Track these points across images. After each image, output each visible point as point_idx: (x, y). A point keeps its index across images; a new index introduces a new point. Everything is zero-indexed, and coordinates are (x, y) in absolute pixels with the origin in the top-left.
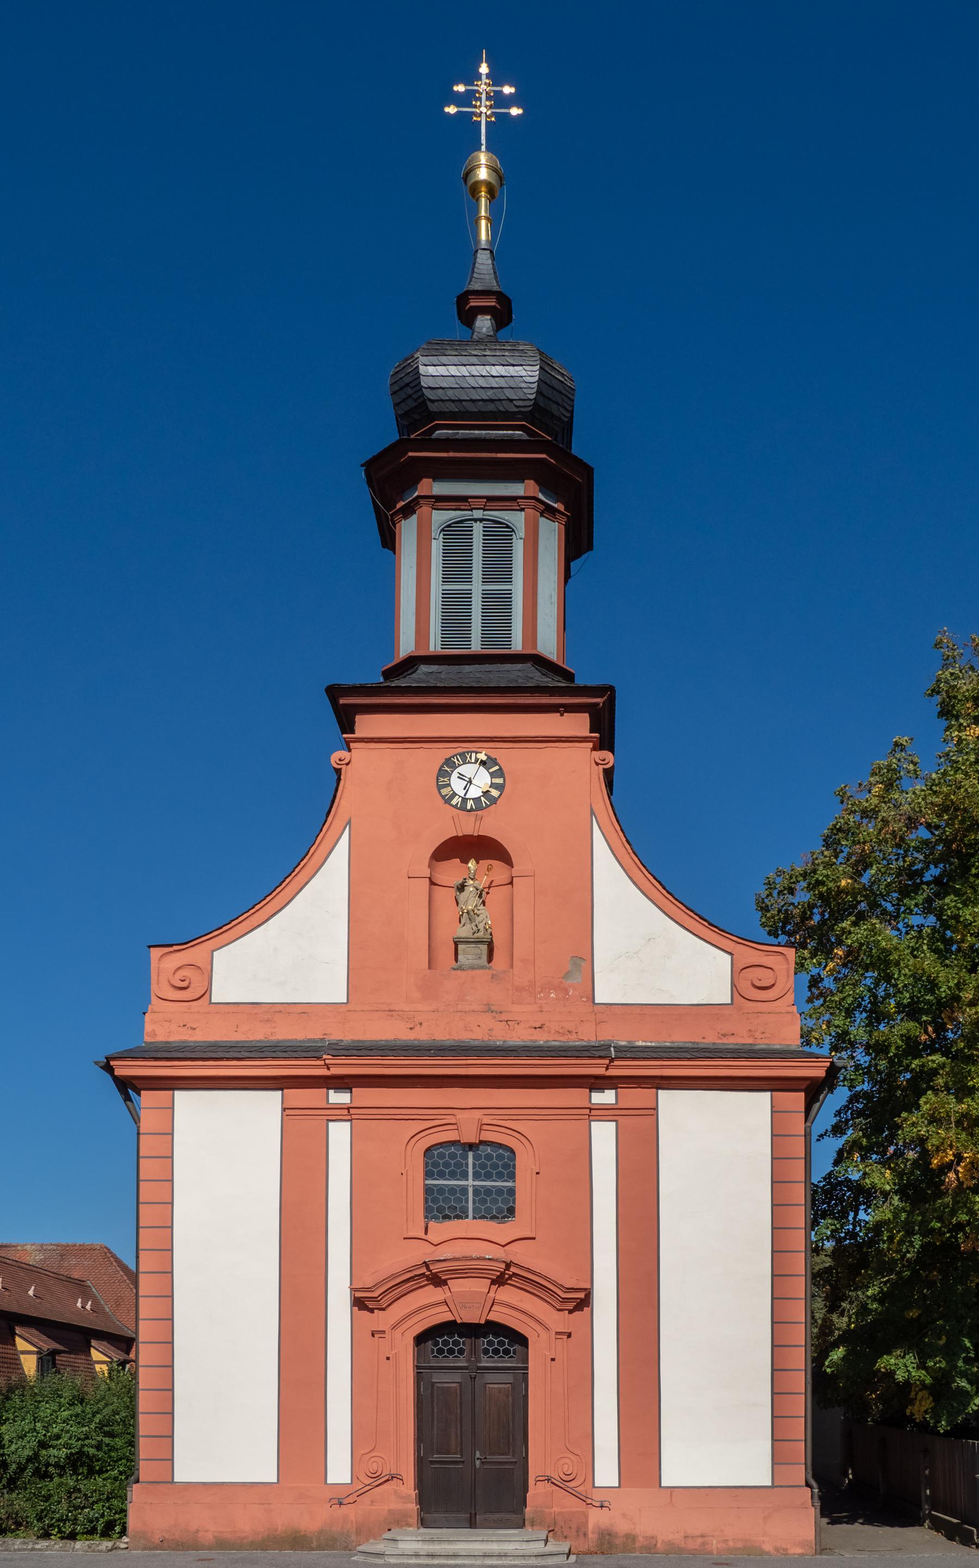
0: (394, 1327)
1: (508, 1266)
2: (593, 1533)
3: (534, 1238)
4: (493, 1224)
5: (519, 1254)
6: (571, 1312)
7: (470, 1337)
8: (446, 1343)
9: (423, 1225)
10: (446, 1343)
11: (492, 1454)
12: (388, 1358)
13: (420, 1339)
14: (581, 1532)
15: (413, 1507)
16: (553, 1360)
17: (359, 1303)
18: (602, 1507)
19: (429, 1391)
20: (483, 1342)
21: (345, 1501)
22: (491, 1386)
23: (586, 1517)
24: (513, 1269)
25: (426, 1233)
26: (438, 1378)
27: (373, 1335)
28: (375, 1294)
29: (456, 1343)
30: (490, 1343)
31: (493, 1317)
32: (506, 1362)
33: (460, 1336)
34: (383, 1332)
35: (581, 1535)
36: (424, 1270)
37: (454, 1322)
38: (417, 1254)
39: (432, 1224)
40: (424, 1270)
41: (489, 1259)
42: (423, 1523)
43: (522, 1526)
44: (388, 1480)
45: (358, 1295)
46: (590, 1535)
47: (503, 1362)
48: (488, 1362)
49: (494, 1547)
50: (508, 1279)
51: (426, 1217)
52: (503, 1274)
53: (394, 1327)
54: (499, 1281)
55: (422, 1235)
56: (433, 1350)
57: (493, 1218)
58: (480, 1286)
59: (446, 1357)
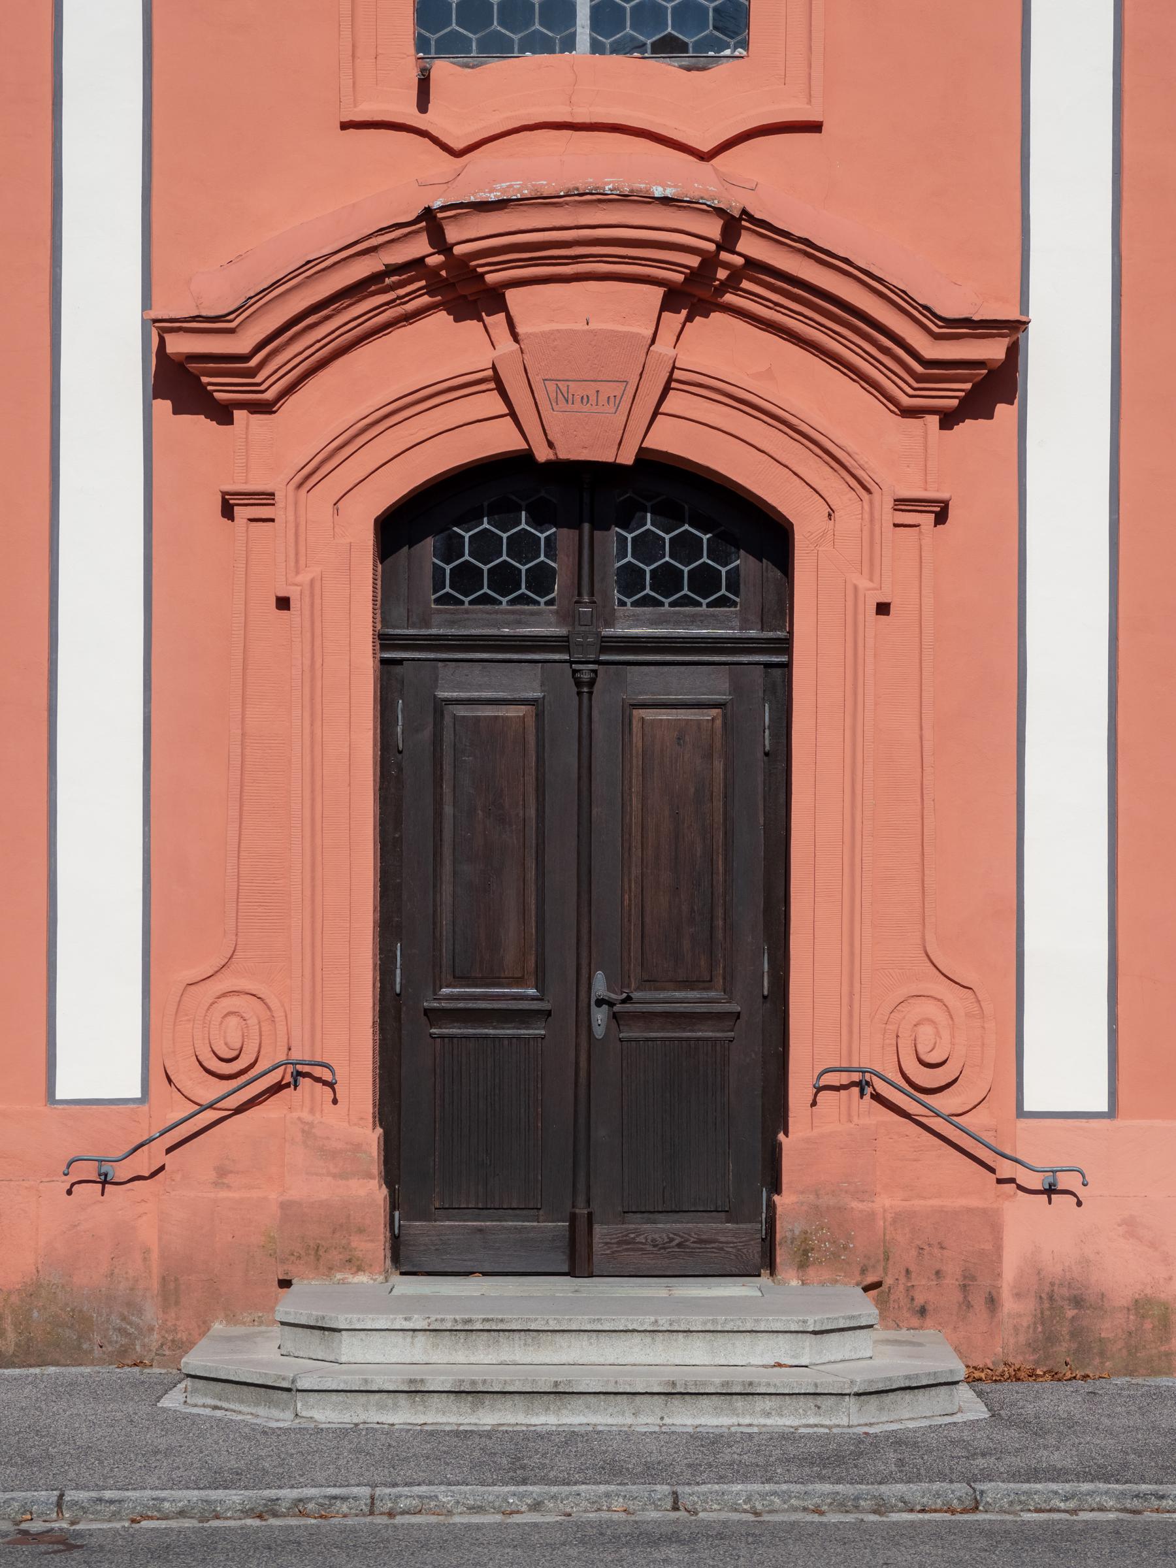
0: (307, 478)
1: (729, 239)
2: (1018, 1295)
3: (815, 127)
4: (666, 70)
5: (762, 181)
6: (949, 420)
7: (577, 526)
8: (486, 546)
9: (413, 76)
10: (486, 546)
11: (650, 982)
12: (283, 603)
13: (397, 528)
14: (977, 1292)
15: (371, 1192)
16: (883, 609)
17: (181, 382)
18: (1050, 1191)
19: (427, 734)
20: (616, 546)
21: (122, 1171)
22: (649, 715)
23: (996, 1229)
24: (750, 246)
25: (423, 104)
26: (467, 686)
27: (228, 511)
28: (240, 344)
29: (523, 546)
30: (647, 547)
31: (668, 438)
32: (701, 620)
33: (538, 521)
34: (268, 497)
35: (978, 1301)
36: (420, 247)
37: (521, 461)
38: (396, 183)
39: (443, 70)
40: (420, 247)
41: (666, 201)
42: (403, 1257)
43: (763, 1259)
44: (278, 1088)
45: (178, 345)
46: (1009, 1305)
47: (693, 620)
48: (638, 621)
49: (695, 1358)
50: (725, 287)
51: (422, 44)
52: (710, 262)
53: (307, 478)
54: (694, 294)
55: (407, 111)
56: (438, 572)
57: (668, 47)
58: (625, 311)
59: (485, 600)
